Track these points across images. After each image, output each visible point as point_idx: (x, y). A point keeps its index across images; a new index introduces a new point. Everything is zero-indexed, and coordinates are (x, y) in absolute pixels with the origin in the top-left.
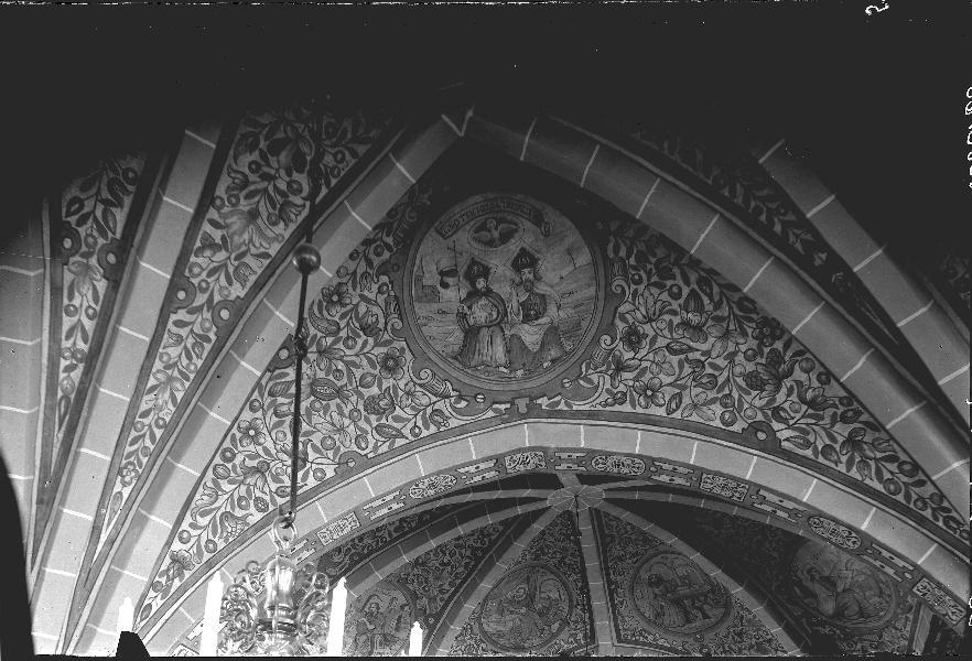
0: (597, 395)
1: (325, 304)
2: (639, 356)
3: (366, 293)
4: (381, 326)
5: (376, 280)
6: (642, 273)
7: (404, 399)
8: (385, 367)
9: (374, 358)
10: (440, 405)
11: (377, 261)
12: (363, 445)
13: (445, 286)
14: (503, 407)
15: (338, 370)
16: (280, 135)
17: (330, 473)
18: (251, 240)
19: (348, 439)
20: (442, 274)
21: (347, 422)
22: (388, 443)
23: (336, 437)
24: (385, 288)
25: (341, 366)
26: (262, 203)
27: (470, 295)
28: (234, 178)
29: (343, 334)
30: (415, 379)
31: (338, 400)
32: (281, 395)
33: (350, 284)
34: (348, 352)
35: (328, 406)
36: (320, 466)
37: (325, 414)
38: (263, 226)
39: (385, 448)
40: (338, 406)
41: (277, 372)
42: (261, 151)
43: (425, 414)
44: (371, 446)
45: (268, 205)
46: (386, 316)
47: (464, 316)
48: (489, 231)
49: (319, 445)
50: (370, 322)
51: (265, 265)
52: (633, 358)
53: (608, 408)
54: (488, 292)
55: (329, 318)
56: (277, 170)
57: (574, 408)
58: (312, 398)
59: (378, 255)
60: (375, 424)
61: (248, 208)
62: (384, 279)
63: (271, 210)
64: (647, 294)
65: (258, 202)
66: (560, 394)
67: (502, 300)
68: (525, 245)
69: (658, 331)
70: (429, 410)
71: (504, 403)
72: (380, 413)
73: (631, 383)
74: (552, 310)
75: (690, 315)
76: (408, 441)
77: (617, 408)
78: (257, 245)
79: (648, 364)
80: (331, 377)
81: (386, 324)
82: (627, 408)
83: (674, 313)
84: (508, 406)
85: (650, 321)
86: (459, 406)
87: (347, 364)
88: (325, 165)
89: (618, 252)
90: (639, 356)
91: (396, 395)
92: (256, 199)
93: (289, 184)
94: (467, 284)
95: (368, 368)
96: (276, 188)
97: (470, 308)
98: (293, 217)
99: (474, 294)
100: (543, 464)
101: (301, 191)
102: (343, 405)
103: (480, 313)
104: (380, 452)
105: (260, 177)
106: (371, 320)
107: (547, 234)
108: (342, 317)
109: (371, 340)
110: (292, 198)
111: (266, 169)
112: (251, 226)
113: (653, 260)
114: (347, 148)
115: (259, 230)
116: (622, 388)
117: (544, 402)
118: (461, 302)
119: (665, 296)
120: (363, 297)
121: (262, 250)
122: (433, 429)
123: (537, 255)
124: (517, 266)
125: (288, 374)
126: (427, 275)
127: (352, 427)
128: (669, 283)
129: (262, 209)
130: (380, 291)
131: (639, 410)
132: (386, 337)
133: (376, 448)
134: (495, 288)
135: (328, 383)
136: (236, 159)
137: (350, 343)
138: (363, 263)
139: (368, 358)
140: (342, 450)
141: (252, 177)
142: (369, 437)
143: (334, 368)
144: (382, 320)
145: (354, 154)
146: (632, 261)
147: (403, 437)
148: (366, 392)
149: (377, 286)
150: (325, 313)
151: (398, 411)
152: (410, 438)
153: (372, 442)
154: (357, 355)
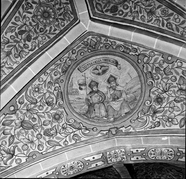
0: (147, 124)
1: (32, 91)
2: (163, 106)
3: (49, 89)
4: (54, 102)
5: (54, 85)
6: (159, 75)
7: (61, 130)
8: (54, 118)
9: (50, 114)
10: (77, 132)
11: (55, 78)
12: (41, 149)
13: (81, 89)
14: (105, 132)
15: (34, 118)
16: (23, 29)
17: (24, 160)
18: (6, 62)
19: (34, 146)
20: (80, 85)
21: (35, 139)
22: (52, 148)
23: (29, 145)
24: (57, 88)
25: (36, 116)
26: (13, 50)
27: (90, 93)
28: (4, 40)
29: (38, 104)
30: (67, 123)
31: (32, 130)
32: (8, 125)
33: (43, 85)
34: (39, 111)
35: (28, 132)
36: (20, 157)
37: (26, 135)
38: (12, 58)
39: (51, 150)
40: (32, 132)
41: (8, 115)
42: (16, 33)
43: (70, 136)
44: (44, 150)
45: (15, 51)
46: (57, 99)
47: (88, 100)
48: (98, 70)
49: (21, 148)
50: (50, 101)
51: (10, 72)
52: (160, 108)
53: (153, 129)
54: (98, 91)
55: (33, 97)
56: (21, 40)
57: (137, 130)
58: (21, 128)
59: (55, 75)
60: (47, 140)
61: (8, 50)
62: (57, 85)
63: (16, 53)
64: (162, 82)
65: (12, 48)
66: (130, 126)
67: (104, 94)
68: (112, 74)
69: (170, 95)
70: (72, 134)
71: (106, 131)
72: (50, 135)
73: (161, 117)
74: (124, 95)
75: (182, 86)
76: (61, 147)
77: (156, 128)
78: (9, 64)
79: (168, 108)
80: (31, 120)
81: (56, 102)
82: (161, 127)
83: (175, 87)
84: (107, 132)
85: (165, 92)
86: (86, 133)
87: (39, 116)
88: (38, 41)
89: (148, 70)
90: (163, 106)
91: (58, 128)
92: (11, 48)
93: (24, 45)
94: (90, 89)
95: (47, 118)
96: (19, 45)
97: (90, 97)
98: (24, 56)
99: (92, 92)
100: (125, 157)
101: (28, 48)
102: (34, 132)
103: (95, 99)
104: (48, 151)
105: (14, 41)
106: (51, 100)
107: (120, 69)
108: (39, 97)
109: (50, 108)
110: (24, 49)
111: (16, 39)
112: (7, 57)
113: (162, 69)
114: (47, 36)
115: (10, 58)
116: (157, 120)
117: (123, 129)
118: (87, 95)
119: (170, 81)
120: (48, 91)
121: (10, 66)
122: (73, 142)
123: (116, 77)
124: (109, 81)
125: (12, 117)
126: (74, 85)
127: (37, 141)
128: (170, 76)
129: (13, 51)
130: (55, 90)
131: (166, 128)
132: (56, 107)
133: (47, 149)
134: (100, 90)
135: (29, 123)
136: (6, 33)
137: (41, 108)
138: (49, 78)
139: (48, 115)
140: (31, 151)
141: (11, 41)
142: (44, 145)
143: (33, 117)
144: (55, 101)
145: (49, 37)
146: (154, 72)
147: (60, 145)
148: (45, 128)
149: (54, 87)
150: (32, 95)
151: (58, 135)
152: (63, 145)
153: (45, 147)
154: (43, 113)
